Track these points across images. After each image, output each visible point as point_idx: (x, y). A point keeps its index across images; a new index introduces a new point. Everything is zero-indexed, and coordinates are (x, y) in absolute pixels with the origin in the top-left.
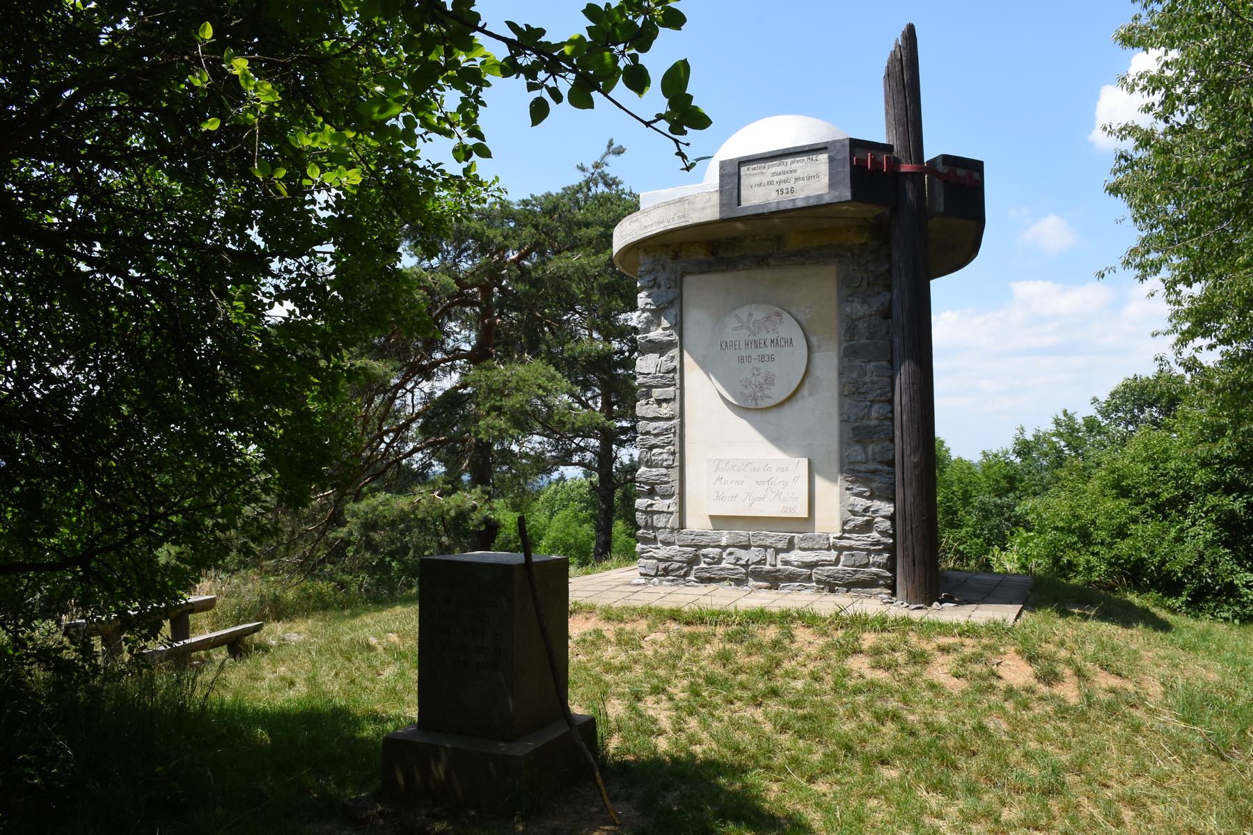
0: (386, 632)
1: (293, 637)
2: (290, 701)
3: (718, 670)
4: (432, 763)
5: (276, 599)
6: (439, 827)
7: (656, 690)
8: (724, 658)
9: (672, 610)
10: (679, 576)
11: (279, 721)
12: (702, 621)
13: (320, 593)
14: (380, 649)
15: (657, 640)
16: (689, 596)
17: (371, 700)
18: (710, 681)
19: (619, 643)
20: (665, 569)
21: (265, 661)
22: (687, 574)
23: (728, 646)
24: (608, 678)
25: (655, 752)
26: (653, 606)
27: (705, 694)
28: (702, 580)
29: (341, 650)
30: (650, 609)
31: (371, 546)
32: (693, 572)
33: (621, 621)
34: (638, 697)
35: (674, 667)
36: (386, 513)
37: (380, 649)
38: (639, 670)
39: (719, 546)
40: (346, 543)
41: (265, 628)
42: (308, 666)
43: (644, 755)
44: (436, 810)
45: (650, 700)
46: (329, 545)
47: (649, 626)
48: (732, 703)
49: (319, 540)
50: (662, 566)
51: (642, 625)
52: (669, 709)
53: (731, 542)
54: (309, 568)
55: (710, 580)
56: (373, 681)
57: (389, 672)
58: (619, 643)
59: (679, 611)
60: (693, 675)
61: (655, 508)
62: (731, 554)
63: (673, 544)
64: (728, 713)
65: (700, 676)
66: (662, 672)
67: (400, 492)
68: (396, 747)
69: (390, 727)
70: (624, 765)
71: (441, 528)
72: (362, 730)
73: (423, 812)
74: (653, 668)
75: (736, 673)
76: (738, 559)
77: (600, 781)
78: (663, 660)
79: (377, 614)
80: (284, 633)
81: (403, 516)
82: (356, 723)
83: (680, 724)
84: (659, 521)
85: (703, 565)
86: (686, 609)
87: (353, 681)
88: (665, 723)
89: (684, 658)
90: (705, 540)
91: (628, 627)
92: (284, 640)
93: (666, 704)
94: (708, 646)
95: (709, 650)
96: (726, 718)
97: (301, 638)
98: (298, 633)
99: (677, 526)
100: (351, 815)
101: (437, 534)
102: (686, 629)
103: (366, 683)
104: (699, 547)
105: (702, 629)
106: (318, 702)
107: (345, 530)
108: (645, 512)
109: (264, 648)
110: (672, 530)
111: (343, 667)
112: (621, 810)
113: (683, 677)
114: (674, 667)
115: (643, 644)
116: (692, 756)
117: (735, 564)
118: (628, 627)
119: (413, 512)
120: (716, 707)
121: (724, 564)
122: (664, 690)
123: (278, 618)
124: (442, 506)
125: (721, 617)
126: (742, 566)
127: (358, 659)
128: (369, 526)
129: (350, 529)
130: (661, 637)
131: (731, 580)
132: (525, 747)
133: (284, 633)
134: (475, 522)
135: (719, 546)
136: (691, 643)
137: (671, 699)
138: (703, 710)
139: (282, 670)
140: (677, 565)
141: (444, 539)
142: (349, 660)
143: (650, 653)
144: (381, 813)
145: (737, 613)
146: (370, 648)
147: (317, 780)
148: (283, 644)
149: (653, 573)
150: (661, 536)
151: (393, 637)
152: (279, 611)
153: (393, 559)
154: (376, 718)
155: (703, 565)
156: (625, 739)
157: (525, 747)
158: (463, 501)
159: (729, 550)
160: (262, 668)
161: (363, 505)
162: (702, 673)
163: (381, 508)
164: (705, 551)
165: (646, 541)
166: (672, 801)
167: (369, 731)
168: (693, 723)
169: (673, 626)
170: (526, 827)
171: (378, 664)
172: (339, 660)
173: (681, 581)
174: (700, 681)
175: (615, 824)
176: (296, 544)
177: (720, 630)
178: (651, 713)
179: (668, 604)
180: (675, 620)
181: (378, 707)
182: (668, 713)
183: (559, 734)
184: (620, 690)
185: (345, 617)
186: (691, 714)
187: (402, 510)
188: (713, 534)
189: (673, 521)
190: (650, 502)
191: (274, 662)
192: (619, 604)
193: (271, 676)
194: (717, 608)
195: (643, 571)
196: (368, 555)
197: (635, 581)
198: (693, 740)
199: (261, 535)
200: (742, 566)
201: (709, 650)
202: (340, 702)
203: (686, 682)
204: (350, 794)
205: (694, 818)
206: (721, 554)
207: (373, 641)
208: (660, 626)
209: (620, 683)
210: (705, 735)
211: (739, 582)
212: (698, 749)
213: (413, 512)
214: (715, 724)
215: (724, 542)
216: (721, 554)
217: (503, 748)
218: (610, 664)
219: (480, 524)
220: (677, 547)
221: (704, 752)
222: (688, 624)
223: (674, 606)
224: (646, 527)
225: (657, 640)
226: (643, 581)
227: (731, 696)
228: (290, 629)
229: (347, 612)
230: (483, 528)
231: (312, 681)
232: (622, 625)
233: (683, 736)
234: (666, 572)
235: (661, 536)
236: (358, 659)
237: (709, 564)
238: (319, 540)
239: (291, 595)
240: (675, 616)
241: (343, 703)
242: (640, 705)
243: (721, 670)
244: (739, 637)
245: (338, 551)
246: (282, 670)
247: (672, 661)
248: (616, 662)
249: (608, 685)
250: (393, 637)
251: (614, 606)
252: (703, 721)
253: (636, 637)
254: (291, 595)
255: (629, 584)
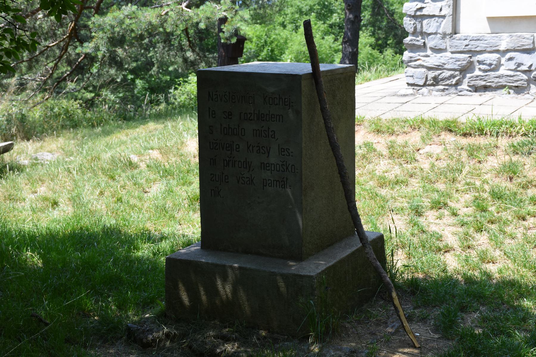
0: (146, 148)
1: (46, 156)
2: (54, 221)
3: (504, 184)
4: (219, 283)
5: (23, 119)
6: (229, 348)
7: (437, 205)
8: (511, 171)
9: (447, 121)
10: (451, 85)
11: (48, 243)
12: (481, 132)
13: (67, 111)
14: (143, 166)
15: (435, 152)
16: (463, 106)
17: (139, 219)
18: (497, 196)
19: (392, 156)
20: (435, 79)
21: (21, 180)
22: (457, 84)
23: (515, 158)
24: (383, 192)
25: (444, 270)
26: (426, 117)
27: (492, 209)
28: (476, 89)
29: (103, 169)
30: (423, 121)
31: (114, 61)
32: (466, 81)
33: (392, 133)
34: (418, 212)
35: (454, 180)
36: (134, 27)
37: (143, 166)
38: (415, 184)
39: (497, 51)
40: (91, 59)
41: (16, 147)
42: (69, 185)
43: (435, 273)
44: (225, 331)
45: (431, 215)
46: (69, 63)
47: (423, 138)
48: (524, 219)
49: (60, 57)
50: (431, 74)
51: (415, 138)
52: (454, 225)
53: (511, 46)
54: (55, 86)
55: (486, 88)
56: (141, 199)
57: (157, 189)
58: (392, 156)
59: (455, 121)
60: (477, 190)
61: (425, 12)
62: (511, 59)
63: (445, 50)
64: (521, 230)
65: (484, 191)
66: (441, 186)
67: (145, 5)
68: (178, 267)
69: (165, 245)
70: (414, 284)
71: (185, 42)
72: (137, 248)
73: (211, 333)
74: (431, 182)
75: (525, 187)
76: (519, 65)
77: (397, 302)
78: (442, 173)
79: (130, 131)
80: (36, 151)
81: (151, 31)
82: (130, 242)
83: (466, 240)
84: (429, 26)
85: (477, 73)
86: (463, 119)
87: (120, 200)
88: (451, 240)
89: (464, 173)
90: (481, 46)
91: (400, 140)
92: (36, 159)
93: (449, 220)
94: (490, 158)
95: (492, 163)
96: (519, 236)
97: (56, 156)
98: (50, 152)
99: (449, 31)
100: (134, 337)
101: (181, 49)
102: (464, 141)
103: (132, 201)
104: (473, 53)
105: (482, 141)
106: (86, 222)
107: (92, 45)
108: (414, 17)
109: (16, 168)
110: (444, 35)
111: (108, 186)
112: (418, 332)
113: (465, 192)
114: (454, 180)
115: (418, 157)
116: (489, 276)
117: (515, 70)
118: (400, 140)
119: (162, 25)
120: (506, 223)
121: (502, 71)
122: (446, 204)
123: (28, 138)
124: (190, 18)
125: (503, 128)
126: (524, 72)
127: (123, 177)
128: (116, 41)
129: (96, 45)
130: (436, 150)
131: (510, 88)
132: (315, 267)
133: (36, 151)
134: (227, 35)
135: (497, 51)
136: (471, 155)
137: (455, 214)
138: (493, 226)
139: (42, 190)
140: (447, 74)
141: (189, 54)
142: (113, 178)
143: (426, 166)
144: (167, 335)
145: (522, 122)
146: (131, 165)
147: (97, 302)
148: (35, 163)
149: (421, 83)
150: (431, 42)
151: (155, 154)
152: (28, 131)
153: (137, 76)
154: (149, 238)
155: (477, 73)
156: (409, 256)
157: (315, 267)
158: (212, 13)
159: (508, 55)
160: (21, 190)
161: (109, 19)
162: (486, 187)
163: (128, 21)
164: (480, 57)
165: (414, 48)
166: (471, 322)
167: (145, 251)
168: (482, 241)
169: (449, 138)
170: (321, 349)
171: (143, 181)
172: (103, 179)
173: (453, 90)
174: (486, 195)
175: (414, 347)
176: (37, 61)
177: (503, 142)
178: (433, 228)
179: (443, 114)
180: (451, 131)
181: (149, 226)
182: (454, 229)
183: (349, 251)
184: (398, 205)
185: (98, 135)
186: (479, 230)
187: (150, 23)
188: (491, 40)
189: (446, 25)
190: (420, 5)
191: (31, 181)
192: (389, 116)
193: (33, 196)
194: (497, 118)
195: (411, 81)
196: (113, 71)
197: (403, 92)
198: (484, 258)
199: (17, 48)
200: (524, 72)
201: (492, 163)
202: (110, 221)
203: (469, 197)
204: (132, 316)
205: (503, 343)
206: (499, 60)
207: (135, 159)
208: (436, 139)
209: (399, 197)
210: (498, 253)
211: (519, 90)
212: (492, 268)
213: (162, 25)
214: (508, 241)
215: (502, 48)
216: (499, 60)
217: (293, 267)
218: (384, 178)
219: (231, 37)
220: (448, 54)
221: (500, 272)
222: (465, 135)
223: (449, 117)
224: (414, 33)
225: (435, 152)
226: (410, 91)
227: (523, 212)
228: (41, 147)
229: (99, 129)
230: (234, 40)
231: (76, 200)
232: (393, 138)
233: (473, 253)
234: (436, 81)
235: (431, 42)
236: (123, 177)
237: (485, 71)
238: (60, 57)
239: (37, 114)
240: (450, 127)
241: (113, 222)
242: (421, 220)
243: (509, 185)
244: (526, 149)
245: (80, 69)
246: (42, 190)
247: (451, 175)
248: (391, 176)
249: (385, 200)
250: (155, 154)
251: (383, 117)
252: (493, 238)
253: (410, 149)
254: (37, 114)
255: (395, 95)
